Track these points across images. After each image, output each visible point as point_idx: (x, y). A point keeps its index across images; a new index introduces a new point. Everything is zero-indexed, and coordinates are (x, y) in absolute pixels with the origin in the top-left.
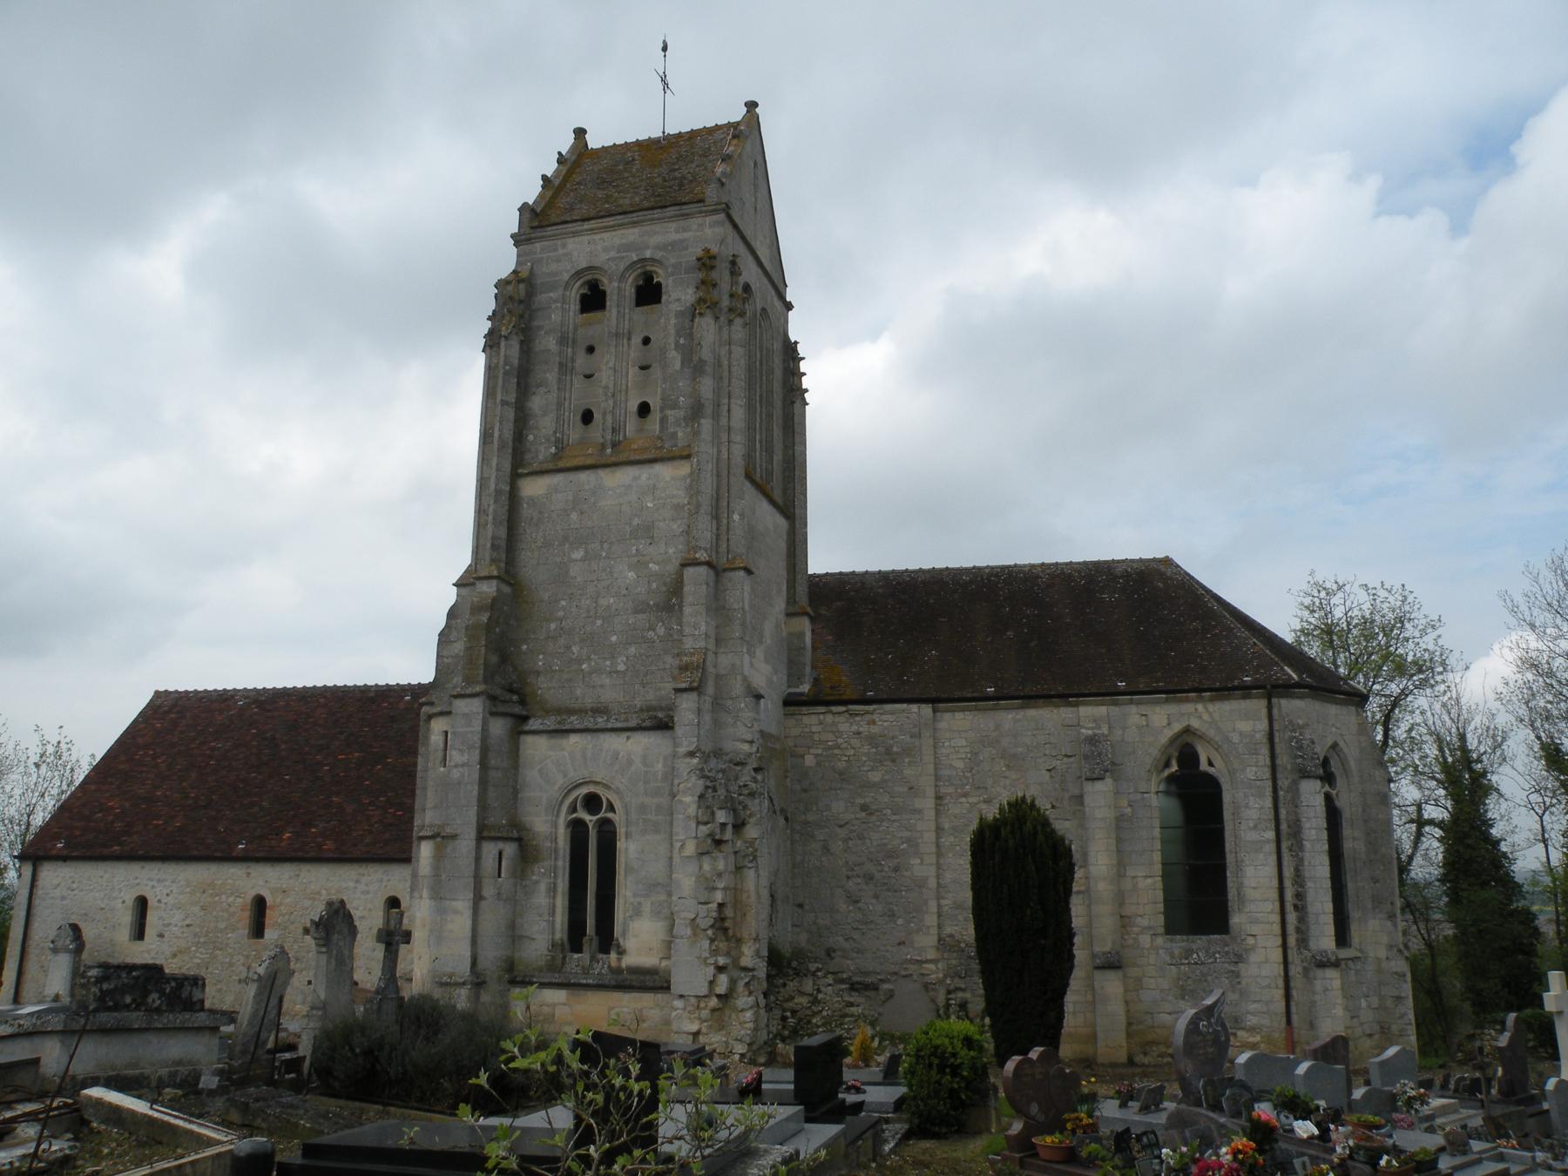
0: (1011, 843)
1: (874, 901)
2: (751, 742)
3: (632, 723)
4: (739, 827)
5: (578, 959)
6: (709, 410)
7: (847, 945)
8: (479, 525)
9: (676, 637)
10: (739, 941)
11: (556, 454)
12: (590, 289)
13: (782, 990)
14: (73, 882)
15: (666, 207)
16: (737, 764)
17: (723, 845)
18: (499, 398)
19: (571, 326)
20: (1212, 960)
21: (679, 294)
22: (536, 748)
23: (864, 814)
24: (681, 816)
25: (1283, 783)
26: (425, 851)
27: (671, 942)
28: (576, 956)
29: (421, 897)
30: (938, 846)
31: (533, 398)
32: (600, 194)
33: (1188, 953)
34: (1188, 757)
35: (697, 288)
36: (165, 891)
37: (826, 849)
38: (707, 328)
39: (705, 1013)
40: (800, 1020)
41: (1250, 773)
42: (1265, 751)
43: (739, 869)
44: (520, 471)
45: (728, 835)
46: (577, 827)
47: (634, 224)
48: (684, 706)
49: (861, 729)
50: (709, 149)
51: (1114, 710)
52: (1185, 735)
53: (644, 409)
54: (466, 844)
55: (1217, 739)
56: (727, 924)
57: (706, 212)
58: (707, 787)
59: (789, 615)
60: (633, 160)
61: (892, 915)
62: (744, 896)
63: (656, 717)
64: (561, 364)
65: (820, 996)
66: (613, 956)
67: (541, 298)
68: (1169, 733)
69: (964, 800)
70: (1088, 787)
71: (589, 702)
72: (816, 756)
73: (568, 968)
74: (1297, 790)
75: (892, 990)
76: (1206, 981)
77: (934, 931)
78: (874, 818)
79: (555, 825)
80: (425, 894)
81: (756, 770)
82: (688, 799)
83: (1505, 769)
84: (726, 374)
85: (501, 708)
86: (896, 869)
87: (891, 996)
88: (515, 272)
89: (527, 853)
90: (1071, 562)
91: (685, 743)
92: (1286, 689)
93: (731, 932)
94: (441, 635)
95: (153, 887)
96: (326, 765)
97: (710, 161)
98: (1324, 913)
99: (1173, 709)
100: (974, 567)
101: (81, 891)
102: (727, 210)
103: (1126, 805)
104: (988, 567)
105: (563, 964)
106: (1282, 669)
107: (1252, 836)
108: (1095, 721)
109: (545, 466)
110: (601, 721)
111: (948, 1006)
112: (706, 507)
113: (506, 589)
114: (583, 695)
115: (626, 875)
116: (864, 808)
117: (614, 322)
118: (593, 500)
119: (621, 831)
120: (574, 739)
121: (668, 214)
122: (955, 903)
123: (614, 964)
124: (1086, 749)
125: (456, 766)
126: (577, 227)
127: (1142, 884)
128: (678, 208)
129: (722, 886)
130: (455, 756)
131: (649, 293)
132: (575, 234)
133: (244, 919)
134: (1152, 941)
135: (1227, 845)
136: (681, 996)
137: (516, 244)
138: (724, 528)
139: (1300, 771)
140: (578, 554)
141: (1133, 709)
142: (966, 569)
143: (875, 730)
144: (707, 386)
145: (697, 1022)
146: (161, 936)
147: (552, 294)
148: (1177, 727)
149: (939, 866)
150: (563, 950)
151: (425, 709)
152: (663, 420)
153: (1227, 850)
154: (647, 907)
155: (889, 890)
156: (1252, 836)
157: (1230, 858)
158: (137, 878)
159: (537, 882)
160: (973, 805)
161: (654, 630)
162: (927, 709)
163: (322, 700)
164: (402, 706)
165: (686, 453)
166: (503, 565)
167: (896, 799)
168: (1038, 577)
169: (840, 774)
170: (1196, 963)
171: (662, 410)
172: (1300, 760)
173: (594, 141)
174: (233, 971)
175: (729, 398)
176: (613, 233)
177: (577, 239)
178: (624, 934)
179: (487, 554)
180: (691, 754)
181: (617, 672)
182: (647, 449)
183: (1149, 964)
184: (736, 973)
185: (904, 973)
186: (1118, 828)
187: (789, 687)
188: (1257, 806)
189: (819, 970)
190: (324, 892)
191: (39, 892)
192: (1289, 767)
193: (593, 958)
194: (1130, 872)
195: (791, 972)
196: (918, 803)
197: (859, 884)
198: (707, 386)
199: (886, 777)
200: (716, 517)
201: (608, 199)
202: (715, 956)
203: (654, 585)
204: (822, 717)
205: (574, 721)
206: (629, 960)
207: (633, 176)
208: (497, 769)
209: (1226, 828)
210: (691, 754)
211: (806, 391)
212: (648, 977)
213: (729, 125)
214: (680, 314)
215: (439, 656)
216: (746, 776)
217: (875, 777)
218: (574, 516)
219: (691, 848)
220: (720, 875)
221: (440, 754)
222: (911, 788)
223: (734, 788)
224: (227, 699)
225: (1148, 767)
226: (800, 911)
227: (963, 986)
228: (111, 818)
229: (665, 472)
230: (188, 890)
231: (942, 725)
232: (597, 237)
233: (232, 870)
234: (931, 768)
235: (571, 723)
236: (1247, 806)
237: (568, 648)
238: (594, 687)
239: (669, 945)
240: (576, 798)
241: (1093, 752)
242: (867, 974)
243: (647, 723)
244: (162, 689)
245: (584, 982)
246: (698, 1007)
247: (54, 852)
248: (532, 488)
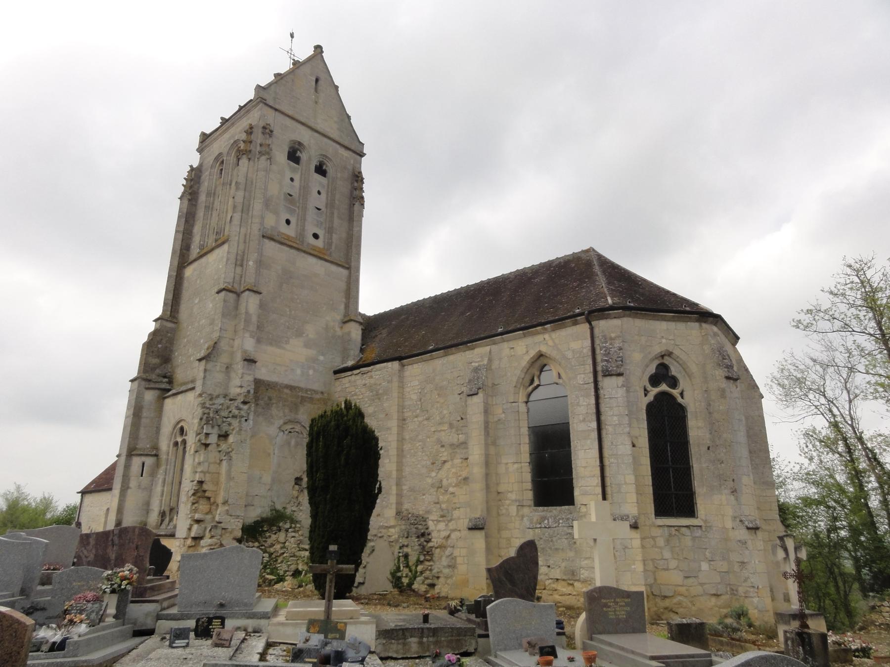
19: (213, 187)
20: (557, 525)
51: (494, 347)
68: (527, 358)
69: (416, 419)
76: (552, 541)
77: (394, 506)
85: (152, 385)
87: (373, 550)
93: (212, 500)
98: (626, 483)
99: (529, 340)
103: (501, 412)
122: (410, 488)
134: (518, 511)
141: (505, 345)
143: (372, 381)
148: (533, 353)
160: (420, 422)
162: (396, 365)
170: (546, 527)
183: (515, 528)
185: (380, 535)
188: (585, 403)
199: (376, 409)
208: (147, 418)
222: (387, 415)
225: (514, 384)
236: (578, 405)
241: (475, 376)
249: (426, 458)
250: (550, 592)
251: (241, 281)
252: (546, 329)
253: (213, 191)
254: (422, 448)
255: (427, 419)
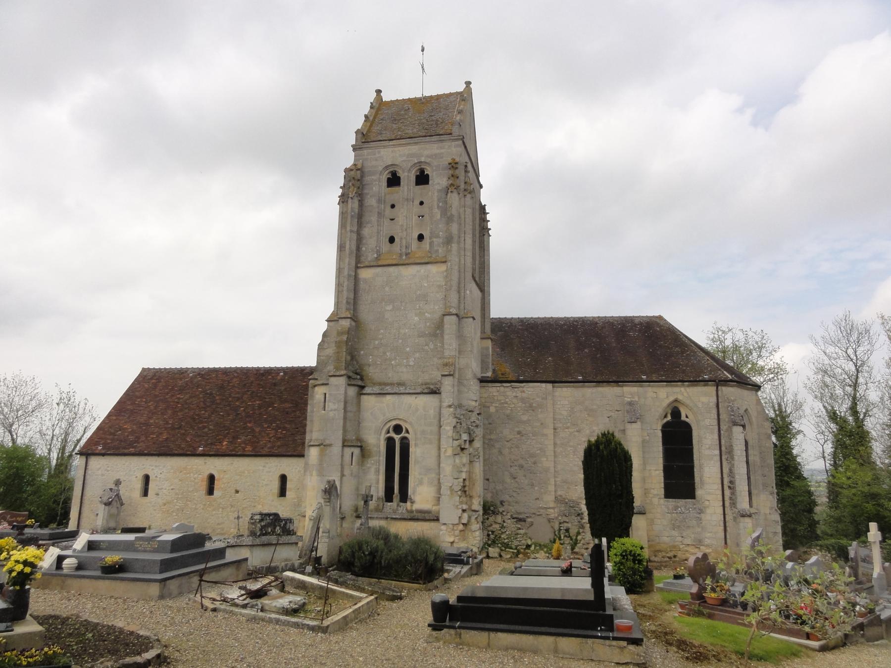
0: (605, 453)
1: (524, 478)
2: (476, 401)
3: (419, 391)
4: (471, 441)
5: (390, 506)
6: (456, 239)
7: (510, 499)
8: (338, 291)
9: (439, 349)
10: (471, 497)
11: (376, 258)
12: (392, 175)
13: (487, 521)
14: (108, 467)
15: (432, 136)
16: (470, 411)
17: (465, 450)
18: (348, 228)
19: (383, 194)
21: (439, 181)
22: (369, 402)
23: (519, 436)
24: (445, 436)
25: (724, 427)
26: (313, 453)
27: (439, 498)
28: (389, 504)
29: (312, 475)
30: (555, 452)
31: (365, 229)
32: (395, 126)
33: (676, 508)
34: (676, 413)
35: (449, 178)
36: (160, 472)
37: (500, 452)
38: (454, 199)
39: (457, 532)
40: (496, 536)
41: (707, 422)
42: (715, 411)
43: (471, 462)
44: (359, 265)
45: (467, 446)
46: (390, 442)
47: (416, 143)
48: (446, 383)
49: (518, 395)
50: (448, 105)
51: (641, 389)
52: (674, 403)
53: (421, 237)
54: (337, 449)
55: (691, 405)
56: (467, 489)
57: (453, 140)
58: (457, 422)
59: (482, 338)
60: (409, 109)
61: (532, 485)
62: (474, 475)
63: (430, 388)
64: (378, 212)
65: (505, 524)
66: (409, 504)
67: (367, 179)
68: (667, 402)
69: (567, 430)
70: (629, 426)
71: (395, 379)
72: (496, 407)
73: (385, 510)
74: (731, 431)
75: (532, 522)
77: (553, 493)
78: (524, 438)
79: (379, 439)
80: (314, 473)
81: (478, 414)
82: (448, 428)
83: (803, 421)
84: (463, 222)
86: (535, 463)
87: (532, 525)
88: (355, 165)
89: (365, 453)
90: (613, 317)
91: (447, 401)
92: (726, 382)
93: (467, 493)
94: (319, 345)
95: (153, 469)
96: (242, 407)
97: (450, 112)
100: (565, 318)
101: (113, 471)
102: (463, 139)
104: (572, 317)
105: (383, 507)
106: (723, 372)
107: (707, 452)
108: (631, 394)
109: (372, 264)
110: (402, 389)
111: (560, 530)
112: (455, 288)
113: (353, 324)
114: (392, 376)
115: (415, 465)
116: (519, 433)
117: (406, 193)
118: (396, 281)
119: (412, 443)
120: (388, 397)
121: (433, 140)
123: (409, 508)
124: (628, 407)
125: (331, 410)
126: (386, 143)
127: (654, 473)
128: (439, 137)
129: (465, 470)
130: (330, 405)
131: (422, 179)
132: (385, 147)
133: (204, 485)
135: (695, 456)
136: (445, 524)
137: (354, 150)
138: (462, 298)
139: (733, 422)
140: (389, 308)
141: (650, 389)
142: (561, 318)
143: (524, 395)
144: (454, 228)
145: (453, 537)
146: (157, 494)
147: (373, 177)
148: (672, 399)
149: (555, 462)
150: (383, 501)
151: (311, 382)
152: (431, 244)
153: (694, 459)
154: (426, 480)
155: (531, 473)
156: (707, 452)
157: (696, 462)
158: (143, 465)
159: (369, 468)
161: (428, 346)
162: (550, 386)
163: (236, 374)
164: (279, 378)
165: (443, 260)
166: (352, 312)
167: (535, 429)
168: (597, 323)
169: (507, 416)
171: (430, 238)
172: (732, 417)
173: (386, 97)
174: (197, 512)
175: (465, 233)
176: (405, 147)
177: (385, 150)
178: (414, 493)
179: (344, 306)
180: (450, 406)
181: (410, 366)
182: (423, 257)
184: (471, 513)
185: (539, 514)
186: (643, 447)
187: (482, 373)
189: (503, 511)
190: (246, 472)
191: (89, 472)
192: (727, 420)
193: (398, 505)
194: (648, 468)
195: (491, 512)
196: (545, 431)
197: (516, 470)
198: (454, 228)
199: (530, 418)
200: (459, 292)
201: (399, 129)
202: (462, 504)
203: (428, 324)
204: (498, 388)
205: (388, 389)
206: (416, 507)
207: (410, 117)
208: (351, 412)
209: (694, 448)
210: (450, 406)
211: (490, 229)
212: (426, 515)
213: (457, 93)
214: (439, 191)
215: (318, 356)
216: (474, 417)
217: (525, 418)
218: (387, 289)
219: (450, 452)
220: (464, 465)
221: (322, 404)
223: (469, 423)
224: (183, 373)
225: (657, 417)
226: (487, 482)
227: (567, 521)
228: (126, 434)
229: (433, 269)
230: (172, 471)
231: (557, 394)
232: (396, 149)
233: (196, 461)
234: (551, 415)
235: (387, 390)
236: (705, 438)
237: (385, 353)
238: (398, 372)
239: (438, 499)
240: (390, 427)
242: (520, 513)
243: (426, 391)
244: (146, 367)
245: (395, 517)
246: (453, 529)
247: (97, 452)
248: (365, 274)
249: (577, 460)
250: (684, 552)
251: (459, 307)
252: (683, 385)
253: (383, 199)
254: (574, 452)
255: (578, 431)
